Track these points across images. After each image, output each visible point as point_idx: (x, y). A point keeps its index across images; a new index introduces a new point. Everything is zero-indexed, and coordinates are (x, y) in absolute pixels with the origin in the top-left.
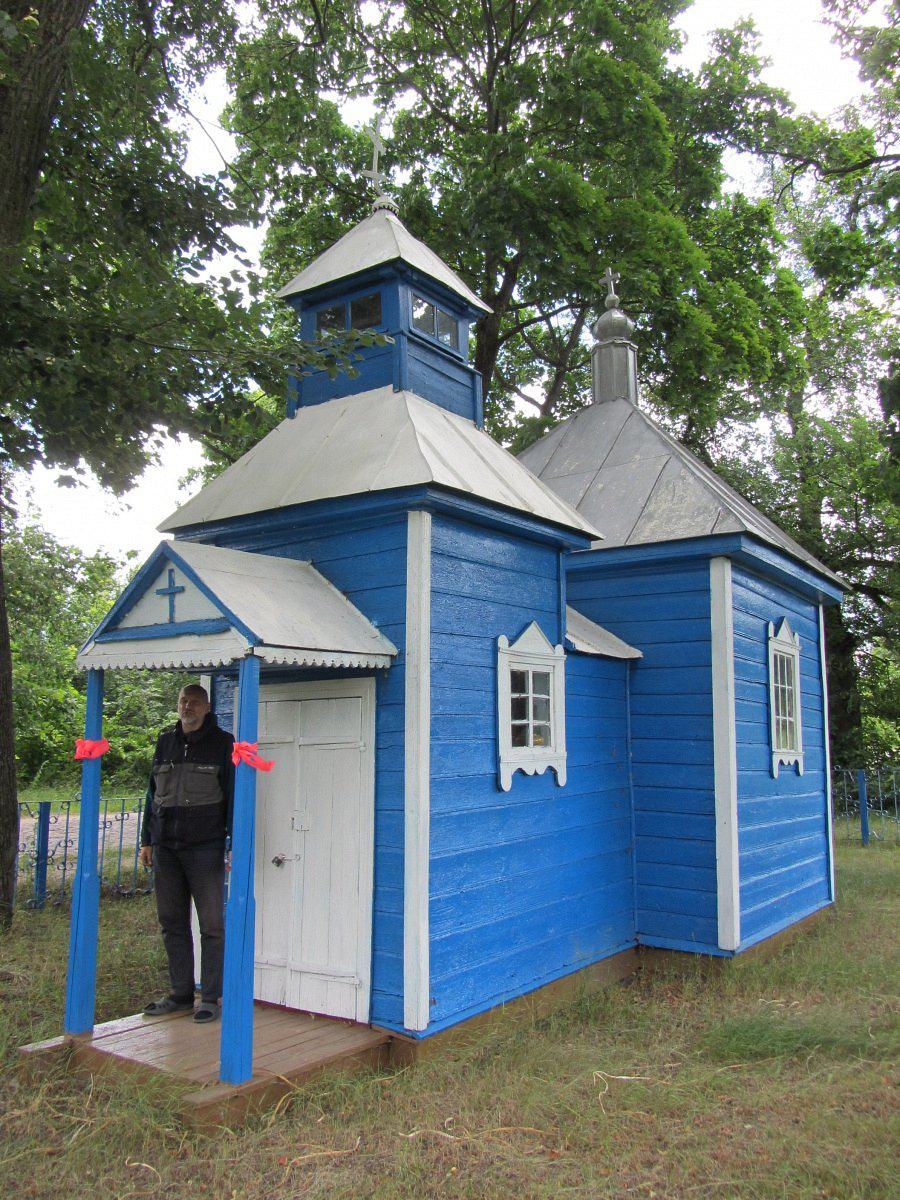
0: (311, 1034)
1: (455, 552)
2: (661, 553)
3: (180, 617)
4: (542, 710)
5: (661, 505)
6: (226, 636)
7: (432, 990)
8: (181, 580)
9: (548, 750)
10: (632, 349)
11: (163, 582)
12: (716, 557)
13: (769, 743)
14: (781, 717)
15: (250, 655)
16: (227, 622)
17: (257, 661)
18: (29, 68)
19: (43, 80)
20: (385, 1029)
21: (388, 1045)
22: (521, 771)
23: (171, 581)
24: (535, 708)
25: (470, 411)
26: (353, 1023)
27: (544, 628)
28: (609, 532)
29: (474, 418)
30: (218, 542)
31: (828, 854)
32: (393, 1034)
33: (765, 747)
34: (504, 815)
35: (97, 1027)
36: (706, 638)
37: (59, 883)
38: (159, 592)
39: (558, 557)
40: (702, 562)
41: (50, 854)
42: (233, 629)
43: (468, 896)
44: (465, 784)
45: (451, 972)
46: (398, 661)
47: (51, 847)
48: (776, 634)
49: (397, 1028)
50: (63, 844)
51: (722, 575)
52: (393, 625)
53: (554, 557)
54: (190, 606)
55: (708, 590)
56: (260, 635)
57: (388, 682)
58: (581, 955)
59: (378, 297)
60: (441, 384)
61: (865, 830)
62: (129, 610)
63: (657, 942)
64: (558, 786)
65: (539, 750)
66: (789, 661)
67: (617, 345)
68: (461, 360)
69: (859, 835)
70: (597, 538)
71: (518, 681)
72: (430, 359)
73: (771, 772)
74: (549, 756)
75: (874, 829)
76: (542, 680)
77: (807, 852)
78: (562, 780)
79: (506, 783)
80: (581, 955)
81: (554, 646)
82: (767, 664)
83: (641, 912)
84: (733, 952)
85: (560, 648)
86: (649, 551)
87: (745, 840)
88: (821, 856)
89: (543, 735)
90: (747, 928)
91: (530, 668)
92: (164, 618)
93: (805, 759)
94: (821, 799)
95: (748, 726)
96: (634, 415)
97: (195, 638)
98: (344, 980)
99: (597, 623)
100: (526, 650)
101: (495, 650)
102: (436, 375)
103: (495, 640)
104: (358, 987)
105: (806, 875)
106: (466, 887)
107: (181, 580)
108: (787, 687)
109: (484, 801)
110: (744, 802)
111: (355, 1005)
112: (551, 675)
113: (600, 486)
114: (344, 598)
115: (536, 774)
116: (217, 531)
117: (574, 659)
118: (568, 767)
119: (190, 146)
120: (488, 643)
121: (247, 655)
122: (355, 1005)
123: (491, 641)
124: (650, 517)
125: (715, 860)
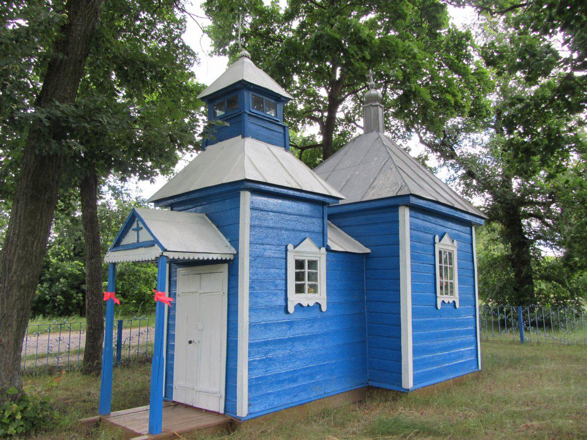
0: (200, 417)
1: (266, 208)
2: (374, 205)
3: (141, 240)
4: (313, 277)
5: (379, 182)
6: (154, 247)
7: (249, 399)
8: (141, 225)
9: (316, 295)
10: (381, 107)
11: (135, 226)
12: (401, 205)
13: (436, 293)
14: (444, 280)
15: (162, 256)
16: (155, 242)
17: (165, 258)
18: (80, 16)
19: (87, 20)
20: (229, 416)
21: (231, 423)
22: (300, 305)
23: (138, 225)
24: (309, 276)
25: (283, 144)
26: (218, 414)
27: (314, 240)
28: (348, 197)
29: (285, 146)
30: (172, 207)
31: (477, 347)
32: (232, 418)
33: (434, 294)
34: (290, 324)
35: (112, 413)
36: (397, 244)
37: (127, 357)
38: (133, 230)
39: (323, 208)
40: (395, 208)
41: (123, 343)
42: (156, 245)
43: (270, 359)
44: (270, 309)
45: (260, 393)
46: (236, 256)
47: (123, 340)
48: (440, 240)
49: (233, 415)
50: (129, 339)
51: (405, 214)
52: (234, 241)
53: (321, 208)
54: (145, 237)
55: (398, 221)
56: (166, 247)
57: (232, 264)
58: (333, 388)
59: (237, 96)
60: (266, 133)
61: (522, 337)
62: (123, 238)
63: (376, 384)
64: (322, 311)
65: (311, 295)
66: (450, 254)
67: (373, 106)
68: (278, 121)
69: (519, 339)
70: (342, 199)
71: (299, 264)
72: (261, 123)
73: (436, 306)
74: (321, 297)
75: (526, 336)
76: (313, 264)
77: (463, 344)
78: (324, 308)
79: (291, 309)
80: (333, 388)
81: (320, 248)
82: (434, 255)
83: (371, 371)
84: (408, 390)
85: (323, 250)
86: (365, 204)
87: (415, 339)
88: (473, 348)
89: (314, 288)
90: (415, 380)
91: (306, 258)
92: (135, 241)
93: (460, 301)
94: (473, 320)
95: (421, 285)
96: (379, 139)
97: (143, 249)
98: (215, 395)
99: (352, 237)
100: (303, 250)
101: (286, 250)
102: (264, 129)
103: (286, 246)
104: (176, 388)
105: (460, 356)
106: (270, 355)
107: (141, 225)
108: (448, 266)
109: (281, 317)
110: (415, 320)
111: (217, 405)
112: (318, 262)
113: (357, 173)
114: (217, 229)
115: (308, 305)
116: (172, 201)
117: (329, 253)
118: (328, 303)
119: (187, 24)
120: (283, 248)
121: (161, 256)
122: (217, 405)
123: (284, 247)
124: (374, 188)
125: (400, 347)
